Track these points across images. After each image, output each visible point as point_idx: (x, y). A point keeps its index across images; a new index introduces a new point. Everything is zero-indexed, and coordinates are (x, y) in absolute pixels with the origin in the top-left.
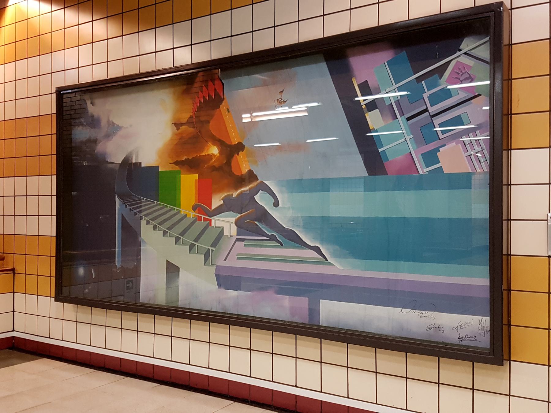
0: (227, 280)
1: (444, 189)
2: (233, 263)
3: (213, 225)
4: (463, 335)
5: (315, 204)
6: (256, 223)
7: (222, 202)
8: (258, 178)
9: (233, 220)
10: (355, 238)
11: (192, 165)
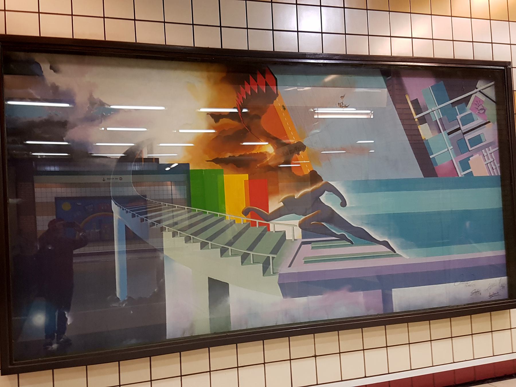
0: (294, 286)
1: (486, 187)
2: (299, 267)
3: (272, 229)
4: (492, 294)
5: (387, 203)
6: (321, 224)
7: (282, 204)
8: (323, 178)
9: (297, 222)
10: (410, 228)
11: (239, 164)
